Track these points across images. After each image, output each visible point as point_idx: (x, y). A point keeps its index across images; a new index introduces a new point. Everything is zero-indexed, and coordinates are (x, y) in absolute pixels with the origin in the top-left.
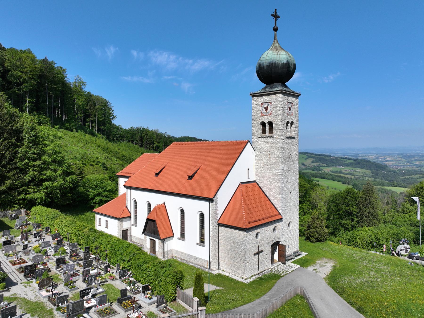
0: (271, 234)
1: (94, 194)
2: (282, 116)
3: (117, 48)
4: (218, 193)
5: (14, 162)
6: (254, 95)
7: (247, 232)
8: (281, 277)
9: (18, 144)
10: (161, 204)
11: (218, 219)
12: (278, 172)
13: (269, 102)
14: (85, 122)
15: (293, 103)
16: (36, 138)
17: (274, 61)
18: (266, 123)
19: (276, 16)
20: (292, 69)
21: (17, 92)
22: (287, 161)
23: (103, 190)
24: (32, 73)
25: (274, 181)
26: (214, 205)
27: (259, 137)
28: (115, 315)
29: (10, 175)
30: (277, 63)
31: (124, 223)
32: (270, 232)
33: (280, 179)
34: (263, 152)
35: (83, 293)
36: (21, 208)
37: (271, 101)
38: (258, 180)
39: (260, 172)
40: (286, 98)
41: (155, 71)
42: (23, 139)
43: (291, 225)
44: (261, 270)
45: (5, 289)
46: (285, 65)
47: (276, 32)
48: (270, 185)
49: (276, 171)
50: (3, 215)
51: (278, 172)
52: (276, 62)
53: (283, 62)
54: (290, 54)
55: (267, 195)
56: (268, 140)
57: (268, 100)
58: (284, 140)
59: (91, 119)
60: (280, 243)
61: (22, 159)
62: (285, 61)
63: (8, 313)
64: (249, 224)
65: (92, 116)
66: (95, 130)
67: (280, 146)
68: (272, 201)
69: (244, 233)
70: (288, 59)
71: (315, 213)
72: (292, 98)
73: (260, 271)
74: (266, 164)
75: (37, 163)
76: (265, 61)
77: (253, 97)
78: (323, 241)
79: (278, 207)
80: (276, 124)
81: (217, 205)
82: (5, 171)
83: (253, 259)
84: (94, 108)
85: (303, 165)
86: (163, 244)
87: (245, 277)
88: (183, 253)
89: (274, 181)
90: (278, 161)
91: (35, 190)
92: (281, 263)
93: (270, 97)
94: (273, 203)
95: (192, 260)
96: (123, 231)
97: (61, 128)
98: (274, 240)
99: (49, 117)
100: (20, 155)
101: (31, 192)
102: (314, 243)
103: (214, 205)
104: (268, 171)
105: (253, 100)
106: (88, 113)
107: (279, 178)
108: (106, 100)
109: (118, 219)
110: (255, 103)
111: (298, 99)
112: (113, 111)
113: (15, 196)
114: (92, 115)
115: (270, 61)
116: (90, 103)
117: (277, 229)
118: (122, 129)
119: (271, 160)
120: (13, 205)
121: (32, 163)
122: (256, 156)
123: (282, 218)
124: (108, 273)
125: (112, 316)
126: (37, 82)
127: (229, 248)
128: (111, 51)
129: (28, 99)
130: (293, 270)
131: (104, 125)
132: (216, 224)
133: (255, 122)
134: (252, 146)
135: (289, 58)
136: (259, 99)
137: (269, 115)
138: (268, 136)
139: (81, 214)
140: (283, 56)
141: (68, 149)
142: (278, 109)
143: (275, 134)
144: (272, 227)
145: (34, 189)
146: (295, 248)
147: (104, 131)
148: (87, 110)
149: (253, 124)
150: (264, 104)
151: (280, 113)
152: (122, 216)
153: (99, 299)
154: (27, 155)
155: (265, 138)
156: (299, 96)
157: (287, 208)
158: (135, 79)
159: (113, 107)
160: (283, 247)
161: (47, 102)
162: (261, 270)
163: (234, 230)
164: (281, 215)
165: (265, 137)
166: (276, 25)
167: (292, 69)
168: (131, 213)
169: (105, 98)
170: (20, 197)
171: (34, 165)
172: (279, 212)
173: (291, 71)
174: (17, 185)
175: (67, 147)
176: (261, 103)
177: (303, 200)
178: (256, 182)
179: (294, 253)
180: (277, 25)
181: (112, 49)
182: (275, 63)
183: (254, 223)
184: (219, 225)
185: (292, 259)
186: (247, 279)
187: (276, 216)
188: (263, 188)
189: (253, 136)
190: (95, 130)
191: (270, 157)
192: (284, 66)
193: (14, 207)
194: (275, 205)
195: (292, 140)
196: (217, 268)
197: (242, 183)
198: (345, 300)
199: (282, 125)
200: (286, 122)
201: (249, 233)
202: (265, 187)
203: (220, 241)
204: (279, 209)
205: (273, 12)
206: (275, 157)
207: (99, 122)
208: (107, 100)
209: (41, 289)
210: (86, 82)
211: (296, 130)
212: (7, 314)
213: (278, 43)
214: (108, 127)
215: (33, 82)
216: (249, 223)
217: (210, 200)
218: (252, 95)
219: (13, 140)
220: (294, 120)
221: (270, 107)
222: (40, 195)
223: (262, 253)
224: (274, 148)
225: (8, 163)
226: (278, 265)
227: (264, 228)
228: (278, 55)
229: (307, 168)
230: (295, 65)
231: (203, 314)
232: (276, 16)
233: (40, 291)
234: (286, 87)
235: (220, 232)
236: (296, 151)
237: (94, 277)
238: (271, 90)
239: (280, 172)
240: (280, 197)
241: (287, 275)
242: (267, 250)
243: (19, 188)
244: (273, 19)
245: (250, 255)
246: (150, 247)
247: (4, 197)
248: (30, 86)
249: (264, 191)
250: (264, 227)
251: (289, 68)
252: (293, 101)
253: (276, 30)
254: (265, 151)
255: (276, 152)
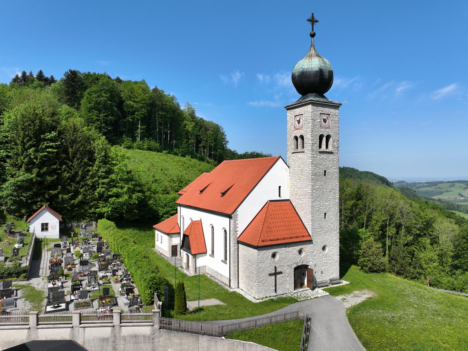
0: (295, 255)
1: (163, 212)
2: (313, 129)
3: (243, 73)
4: (238, 210)
5: (86, 179)
6: (289, 108)
7: (259, 250)
8: (298, 301)
9: (91, 163)
10: (198, 221)
11: (238, 236)
12: (308, 189)
13: (301, 115)
14: (197, 147)
15: (330, 115)
16: (106, 158)
17: (305, 70)
18: (298, 137)
19: (313, 21)
20: (327, 77)
21: (130, 120)
22: (320, 178)
23: (171, 209)
24: (143, 102)
25: (305, 200)
26: (233, 222)
27: (293, 153)
28: (88, 308)
29: (81, 190)
30: (308, 71)
31: (173, 239)
32: (294, 254)
33: (310, 198)
34: (296, 169)
35: (74, 288)
36: (93, 220)
37: (302, 113)
38: (292, 199)
39: (293, 190)
40: (318, 109)
41: (281, 94)
42: (95, 160)
43: (327, 249)
44: (279, 292)
45: (25, 279)
46: (317, 73)
47: (312, 38)
48: (302, 204)
49: (307, 189)
50: (77, 226)
51: (308, 189)
52: (307, 70)
53: (314, 70)
54: (325, 59)
55: (300, 215)
56: (300, 156)
57: (300, 112)
58: (315, 155)
59: (203, 145)
60: (309, 267)
61: (92, 177)
62: (317, 69)
63: (4, 294)
64: (262, 243)
65: (203, 142)
66: (207, 155)
67: (310, 161)
68: (303, 221)
69: (255, 251)
70: (320, 66)
71: (163, 209)
72: (327, 109)
73: (278, 293)
74: (298, 181)
75: (106, 181)
76: (296, 71)
77: (288, 109)
78: (379, 272)
79: (308, 228)
80: (306, 138)
81: (237, 222)
82: (79, 187)
83: (268, 279)
84: (205, 134)
85: (460, 196)
86: (195, 259)
87: (257, 297)
88: (213, 270)
89: (305, 200)
90: (308, 178)
91: (104, 205)
92: (309, 289)
93: (302, 109)
94: (304, 224)
95: (219, 278)
96: (172, 246)
97: (169, 153)
98: (299, 263)
99: (159, 143)
100: (91, 173)
101: (101, 206)
102: (367, 273)
103: (233, 222)
104: (300, 189)
105: (287, 113)
106: (200, 138)
107: (309, 196)
108: (217, 125)
109: (168, 234)
110: (289, 116)
111: (338, 109)
112: (225, 136)
113: (87, 209)
114: (204, 140)
115: (301, 70)
116: (203, 129)
117: (304, 251)
118: (237, 154)
119: (303, 177)
120: (85, 217)
121: (101, 181)
122: (290, 173)
123: (311, 239)
124: (116, 276)
125: (84, 309)
126: (147, 111)
127: (245, 266)
128: (237, 76)
129: (139, 126)
130: (317, 297)
131: (215, 150)
132: (235, 241)
133: (289, 137)
134: (286, 164)
135: (322, 65)
136: (293, 112)
137: (301, 128)
138: (299, 151)
139: (148, 230)
140: (315, 63)
141: (168, 172)
142: (308, 121)
143: (305, 148)
144: (297, 249)
145: (103, 204)
146: (333, 275)
147: (215, 156)
148: (199, 135)
149: (288, 139)
150: (297, 116)
151: (310, 126)
152: (171, 232)
153: (80, 293)
154: (98, 173)
155: (297, 154)
156: (340, 106)
157: (320, 230)
158: (262, 103)
159: (225, 132)
160: (311, 271)
161: (157, 129)
162: (279, 292)
163: (249, 248)
164: (311, 237)
165: (297, 152)
166: (313, 30)
167: (327, 77)
168: (180, 229)
169: (217, 124)
170: (91, 211)
171: (102, 182)
172: (309, 233)
173: (326, 79)
174: (88, 200)
175: (167, 170)
176: (295, 116)
177: (423, 234)
178: (290, 201)
179: (331, 280)
180: (314, 31)
181: (238, 74)
182: (306, 72)
183: (269, 242)
184: (239, 242)
185: (327, 286)
186: (258, 299)
187: (303, 237)
188: (296, 207)
189: (288, 152)
190: (207, 156)
191: (301, 174)
192: (315, 74)
193: (86, 219)
194: (306, 226)
195: (329, 155)
196: (237, 286)
197: (271, 201)
198: (355, 332)
199: (312, 139)
200: (319, 135)
201: (262, 251)
202: (297, 206)
203: (239, 259)
204: (309, 231)
205: (309, 16)
206: (306, 173)
207: (210, 147)
208: (219, 125)
209: (50, 282)
210: (195, 109)
211: (335, 144)
212: (3, 294)
213: (315, 50)
214: (220, 152)
215: (144, 110)
216: (263, 241)
217: (230, 217)
218: (287, 108)
219: (86, 160)
220: (331, 133)
221: (302, 120)
222: (106, 210)
223: (282, 274)
224: (305, 164)
225: (81, 181)
226: (304, 291)
227: (284, 249)
228: (310, 63)
229: (465, 199)
230: (331, 73)
231: (156, 316)
232: (313, 21)
233: (48, 283)
234: (324, 97)
235: (239, 249)
236: (335, 168)
237: (93, 276)
238: (304, 101)
239: (310, 190)
240: (310, 217)
241: (306, 301)
242: (288, 273)
243: (90, 203)
244: (309, 24)
245: (263, 275)
246: (186, 262)
247: (77, 210)
248: (142, 114)
249: (297, 211)
250: (284, 247)
251: (323, 76)
252: (330, 112)
253: (313, 35)
254: (298, 167)
255: (307, 168)
